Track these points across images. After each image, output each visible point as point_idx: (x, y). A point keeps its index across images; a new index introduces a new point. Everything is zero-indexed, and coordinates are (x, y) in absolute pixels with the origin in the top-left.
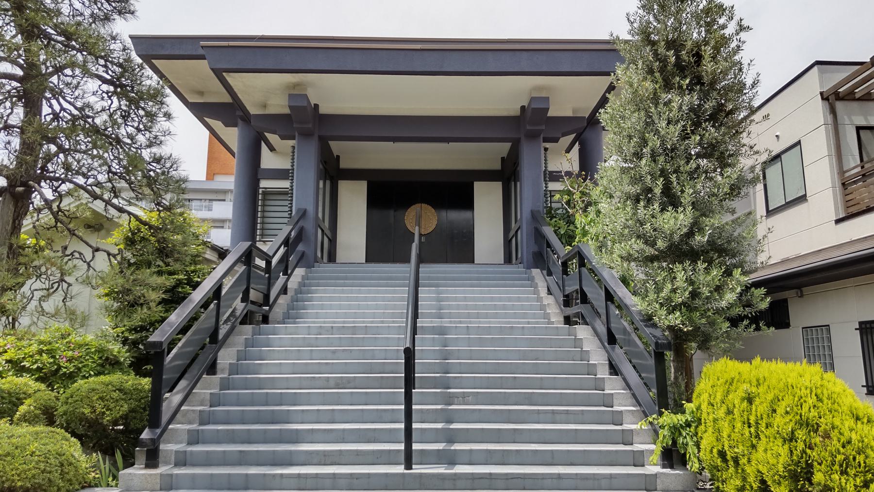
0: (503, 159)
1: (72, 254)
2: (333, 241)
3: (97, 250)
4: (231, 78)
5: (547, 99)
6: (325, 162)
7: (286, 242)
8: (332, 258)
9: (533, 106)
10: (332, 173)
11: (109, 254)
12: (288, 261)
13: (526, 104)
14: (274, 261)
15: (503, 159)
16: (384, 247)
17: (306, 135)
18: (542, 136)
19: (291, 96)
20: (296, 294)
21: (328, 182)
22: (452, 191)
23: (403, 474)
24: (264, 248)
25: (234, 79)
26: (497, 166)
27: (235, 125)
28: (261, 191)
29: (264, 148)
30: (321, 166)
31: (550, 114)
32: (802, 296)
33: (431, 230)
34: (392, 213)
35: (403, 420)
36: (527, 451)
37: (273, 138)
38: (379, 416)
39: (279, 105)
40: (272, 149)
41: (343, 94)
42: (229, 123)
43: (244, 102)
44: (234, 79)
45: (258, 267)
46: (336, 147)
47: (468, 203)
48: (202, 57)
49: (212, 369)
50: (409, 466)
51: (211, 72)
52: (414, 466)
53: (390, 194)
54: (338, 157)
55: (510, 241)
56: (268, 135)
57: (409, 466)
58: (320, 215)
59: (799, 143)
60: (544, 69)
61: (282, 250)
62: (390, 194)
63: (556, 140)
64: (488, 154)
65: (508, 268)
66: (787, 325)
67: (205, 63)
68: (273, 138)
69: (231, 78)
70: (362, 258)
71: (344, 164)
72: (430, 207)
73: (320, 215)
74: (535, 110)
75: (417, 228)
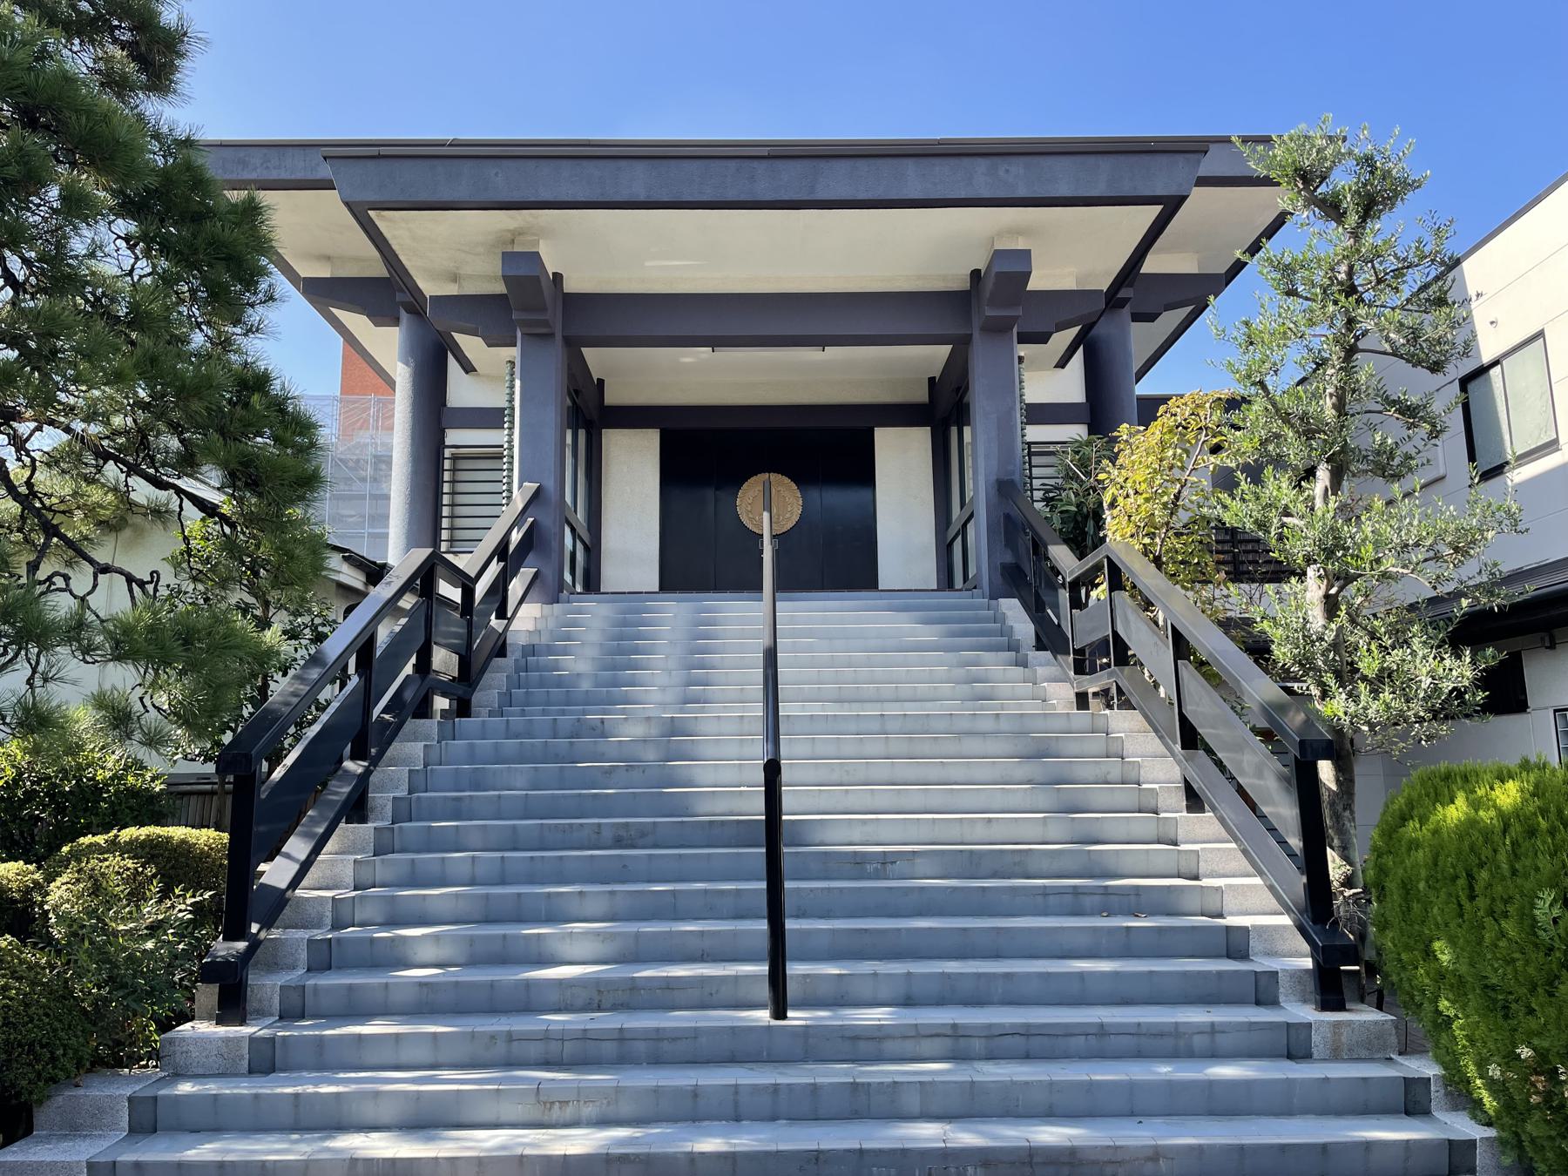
0: (931, 380)
1: (49, 579)
2: (593, 550)
3: (106, 569)
4: (386, 222)
5: (1026, 254)
6: (576, 392)
7: (501, 551)
8: (592, 583)
9: (996, 269)
10: (591, 415)
11: (130, 579)
12: (506, 590)
13: (981, 265)
14: (481, 589)
15: (931, 380)
16: (701, 558)
17: (538, 336)
18: (1015, 330)
19: (508, 257)
20: (524, 655)
21: (582, 434)
22: (829, 450)
23: (769, 1027)
24: (461, 562)
25: (392, 225)
26: (921, 395)
27: (396, 322)
28: (447, 453)
29: (453, 365)
30: (569, 402)
31: (1034, 284)
32: (1552, 646)
33: (796, 518)
34: (710, 494)
35: (765, 912)
36: (1028, 974)
37: (471, 345)
38: (708, 908)
39: (484, 278)
40: (468, 368)
41: (605, 251)
42: (382, 315)
43: (412, 272)
44: (392, 225)
45: (447, 602)
46: (594, 357)
47: (863, 474)
48: (327, 185)
49: (357, 809)
50: (780, 1014)
51: (346, 209)
52: (790, 1014)
53: (707, 455)
54: (601, 382)
55: (950, 545)
56: (460, 338)
57: (780, 1014)
58: (568, 499)
59: (1540, 334)
60: (1022, 192)
61: (495, 568)
62: (707, 455)
63: (1043, 338)
64: (915, 363)
65: (948, 598)
66: (1520, 706)
67: (332, 196)
68: (471, 345)
69: (386, 222)
70: (653, 583)
71: (612, 397)
72: (787, 480)
73: (568, 499)
74: (1001, 276)
75: (766, 515)
